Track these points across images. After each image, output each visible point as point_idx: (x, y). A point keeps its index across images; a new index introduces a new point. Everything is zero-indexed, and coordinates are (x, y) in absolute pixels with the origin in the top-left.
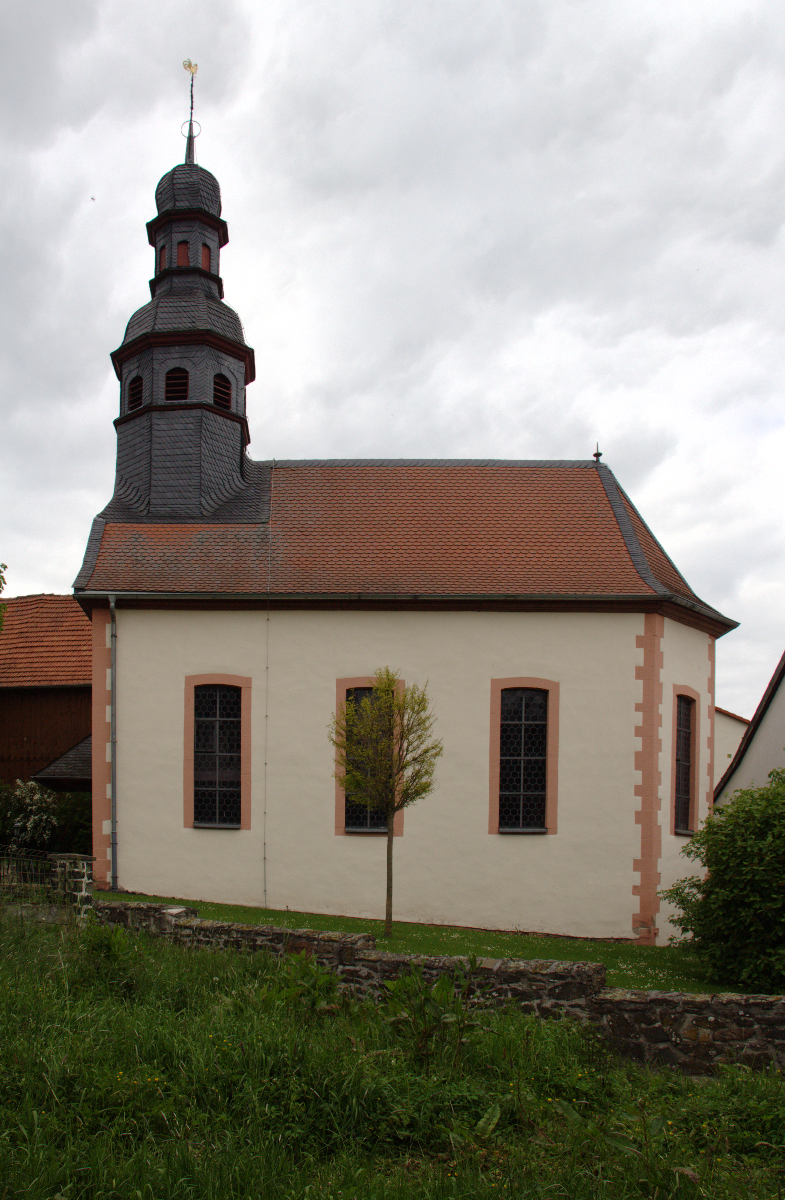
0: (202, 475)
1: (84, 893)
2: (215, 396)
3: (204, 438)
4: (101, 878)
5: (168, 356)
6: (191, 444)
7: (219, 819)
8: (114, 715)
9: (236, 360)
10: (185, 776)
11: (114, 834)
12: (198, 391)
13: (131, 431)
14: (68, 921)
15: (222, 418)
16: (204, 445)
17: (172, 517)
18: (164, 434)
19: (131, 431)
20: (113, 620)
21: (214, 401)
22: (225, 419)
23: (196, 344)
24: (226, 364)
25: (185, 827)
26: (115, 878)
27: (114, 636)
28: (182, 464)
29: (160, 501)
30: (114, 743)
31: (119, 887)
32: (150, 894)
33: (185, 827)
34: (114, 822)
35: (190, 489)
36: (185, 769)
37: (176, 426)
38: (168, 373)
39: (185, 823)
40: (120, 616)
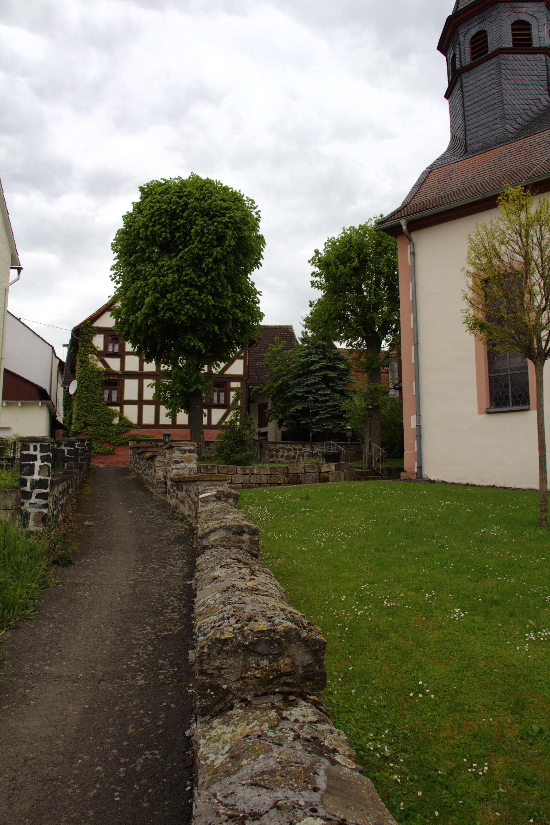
0: (505, 106)
1: (36, 477)
2: (514, 40)
3: (504, 77)
4: (411, 469)
5: (470, 26)
6: (494, 86)
7: (512, 402)
8: (416, 320)
9: (535, 4)
10: (477, 364)
11: (419, 427)
12: (495, 42)
13: (453, 98)
14: (12, 506)
15: (523, 56)
16: (505, 82)
17: (482, 149)
18: (472, 87)
19: (453, 98)
20: (410, 240)
21: (513, 44)
22: (526, 56)
23: (491, 6)
24: (524, 10)
25: (479, 413)
26: (420, 468)
27: (413, 254)
28: (488, 104)
29: (474, 140)
30: (416, 344)
31: (424, 476)
32: (450, 481)
33: (479, 413)
34: (419, 417)
35: (497, 121)
36: (477, 358)
37: (481, 77)
38: (472, 39)
39: (479, 410)
40: (414, 236)
